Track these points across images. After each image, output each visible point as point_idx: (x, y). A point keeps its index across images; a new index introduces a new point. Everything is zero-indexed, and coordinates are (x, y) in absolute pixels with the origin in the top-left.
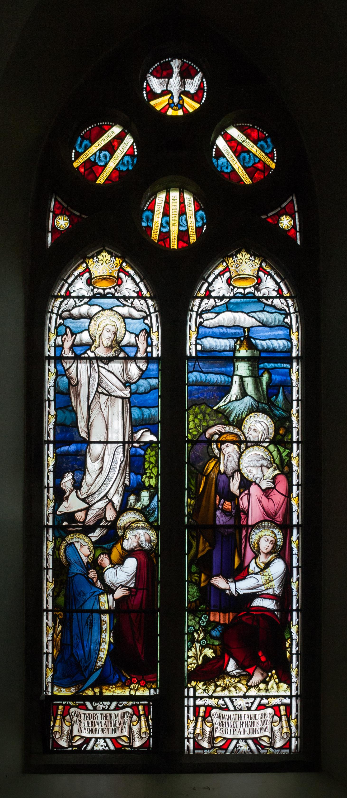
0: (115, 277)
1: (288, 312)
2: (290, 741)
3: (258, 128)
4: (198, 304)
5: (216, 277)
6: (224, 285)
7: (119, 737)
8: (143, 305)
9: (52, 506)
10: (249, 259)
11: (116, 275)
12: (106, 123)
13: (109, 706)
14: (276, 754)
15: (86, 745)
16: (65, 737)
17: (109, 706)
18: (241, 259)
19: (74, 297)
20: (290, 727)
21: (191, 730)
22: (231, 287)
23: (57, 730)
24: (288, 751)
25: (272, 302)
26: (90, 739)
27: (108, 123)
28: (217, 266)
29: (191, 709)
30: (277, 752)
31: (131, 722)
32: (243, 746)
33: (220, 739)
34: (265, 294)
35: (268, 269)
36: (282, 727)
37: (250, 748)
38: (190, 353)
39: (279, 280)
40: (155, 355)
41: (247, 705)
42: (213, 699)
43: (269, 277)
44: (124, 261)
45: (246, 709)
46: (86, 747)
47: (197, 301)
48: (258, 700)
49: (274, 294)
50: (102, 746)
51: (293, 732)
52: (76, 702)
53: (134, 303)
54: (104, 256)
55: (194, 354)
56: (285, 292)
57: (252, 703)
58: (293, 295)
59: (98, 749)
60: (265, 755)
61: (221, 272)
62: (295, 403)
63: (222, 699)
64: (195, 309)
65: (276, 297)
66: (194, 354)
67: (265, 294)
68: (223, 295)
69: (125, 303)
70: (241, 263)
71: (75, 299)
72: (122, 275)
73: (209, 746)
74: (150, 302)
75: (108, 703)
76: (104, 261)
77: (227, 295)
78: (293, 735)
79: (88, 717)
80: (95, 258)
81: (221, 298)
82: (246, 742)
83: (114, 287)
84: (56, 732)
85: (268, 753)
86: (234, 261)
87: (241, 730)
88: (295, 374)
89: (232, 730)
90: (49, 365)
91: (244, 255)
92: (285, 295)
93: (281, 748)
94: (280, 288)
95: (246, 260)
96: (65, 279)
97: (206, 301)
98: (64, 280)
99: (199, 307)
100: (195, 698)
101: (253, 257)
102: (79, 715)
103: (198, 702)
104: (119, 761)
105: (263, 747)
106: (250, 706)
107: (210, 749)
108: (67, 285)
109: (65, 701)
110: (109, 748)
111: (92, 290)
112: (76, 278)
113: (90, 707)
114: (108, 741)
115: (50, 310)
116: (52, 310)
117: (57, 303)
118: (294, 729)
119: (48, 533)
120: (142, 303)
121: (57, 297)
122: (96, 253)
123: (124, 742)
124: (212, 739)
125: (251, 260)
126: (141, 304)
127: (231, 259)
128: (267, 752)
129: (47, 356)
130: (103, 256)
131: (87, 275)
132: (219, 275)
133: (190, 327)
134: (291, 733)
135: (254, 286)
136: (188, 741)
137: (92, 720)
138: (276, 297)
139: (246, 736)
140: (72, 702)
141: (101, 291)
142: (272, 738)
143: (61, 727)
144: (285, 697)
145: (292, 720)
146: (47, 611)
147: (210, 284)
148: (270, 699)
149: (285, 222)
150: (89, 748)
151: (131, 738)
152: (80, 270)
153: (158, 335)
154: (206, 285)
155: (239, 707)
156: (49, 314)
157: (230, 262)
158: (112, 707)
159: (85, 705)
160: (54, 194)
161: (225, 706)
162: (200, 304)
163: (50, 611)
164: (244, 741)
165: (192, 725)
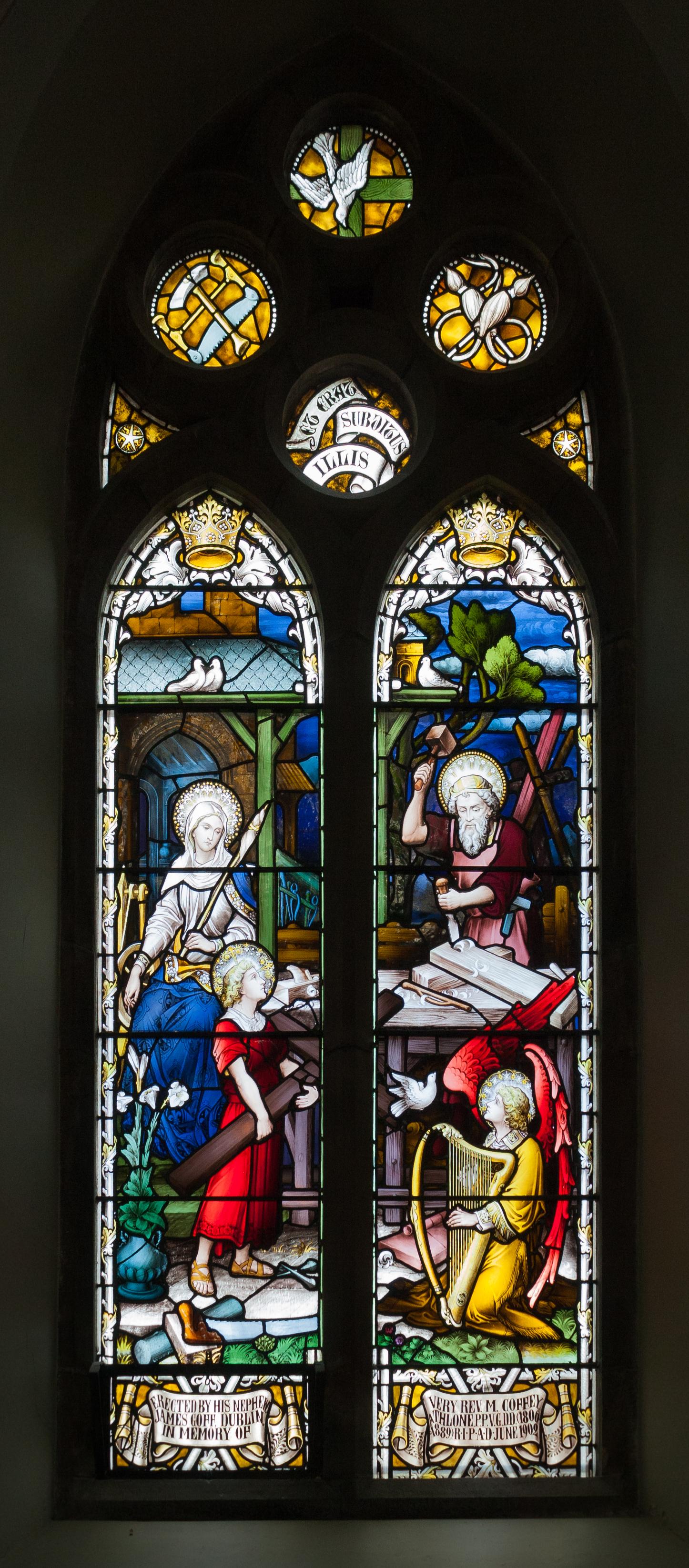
1: (296, 616)
2: (577, 1450)
4: (395, 601)
5: (431, 548)
6: (448, 564)
8: (560, 601)
9: (113, 994)
13: (223, 1386)
14: (551, 1478)
15: (181, 1461)
17: (223, 1386)
18: (204, 514)
19: (152, 589)
20: (577, 1426)
21: (385, 1432)
23: (401, 1435)
24: (572, 1473)
26: (190, 1449)
28: (156, 531)
29: (385, 1390)
30: (553, 1474)
31: (268, 1416)
33: (164, 1448)
37: (499, 1467)
38: (379, 698)
39: (277, 556)
40: (311, 700)
41: (494, 1382)
42: (427, 1370)
43: (259, 550)
44: (249, 518)
45: (491, 1390)
46: (182, 1465)
47: (121, 596)
48: (515, 1371)
49: (270, 582)
51: (583, 1434)
52: (160, 1378)
53: (268, 598)
54: (484, 505)
55: (386, 698)
56: (565, 578)
57: (504, 1378)
58: (304, 583)
59: (204, 1469)
60: (530, 1480)
61: (439, 538)
62: (585, 794)
63: (443, 1371)
64: (391, 611)
66: (386, 698)
68: (445, 582)
69: (525, 596)
70: (479, 521)
71: (155, 593)
73: (420, 1463)
74: (574, 596)
75: (222, 1379)
76: (484, 514)
77: (452, 581)
78: (584, 1441)
79: (189, 1406)
81: (441, 588)
82: (492, 1454)
85: (535, 1476)
89: (467, 1430)
90: (105, 719)
91: (210, 507)
92: (564, 585)
93: (560, 1466)
95: (215, 518)
96: (134, 551)
97: (411, 593)
98: (131, 553)
99: (399, 605)
100: (393, 1368)
101: (228, 510)
103: (399, 1377)
106: (498, 1383)
107: (422, 1468)
108: (137, 565)
109: (137, 1375)
110: (225, 1467)
111: (188, 575)
112: (154, 552)
113: (186, 1388)
114: (223, 1452)
115: (106, 612)
118: (584, 1430)
119: (104, 1047)
120: (284, 598)
121: (119, 588)
122: (194, 500)
123: (255, 1455)
125: (498, 516)
126: (557, 600)
127: (186, 514)
129: (101, 702)
130: (207, 507)
133: (105, 649)
134: (580, 1438)
135: (503, 566)
140: (150, 1378)
142: (267, 1447)
144: (567, 1366)
146: (104, 1199)
148: (537, 1372)
149: (566, 444)
150: (188, 1465)
151: (267, 1447)
152: (163, 535)
153: (317, 661)
154: (413, 562)
155: (478, 1387)
156: (105, 619)
157: (183, 521)
158: (230, 1388)
159: (175, 1382)
161: (451, 1385)
163: (109, 1199)
164: (488, 1451)
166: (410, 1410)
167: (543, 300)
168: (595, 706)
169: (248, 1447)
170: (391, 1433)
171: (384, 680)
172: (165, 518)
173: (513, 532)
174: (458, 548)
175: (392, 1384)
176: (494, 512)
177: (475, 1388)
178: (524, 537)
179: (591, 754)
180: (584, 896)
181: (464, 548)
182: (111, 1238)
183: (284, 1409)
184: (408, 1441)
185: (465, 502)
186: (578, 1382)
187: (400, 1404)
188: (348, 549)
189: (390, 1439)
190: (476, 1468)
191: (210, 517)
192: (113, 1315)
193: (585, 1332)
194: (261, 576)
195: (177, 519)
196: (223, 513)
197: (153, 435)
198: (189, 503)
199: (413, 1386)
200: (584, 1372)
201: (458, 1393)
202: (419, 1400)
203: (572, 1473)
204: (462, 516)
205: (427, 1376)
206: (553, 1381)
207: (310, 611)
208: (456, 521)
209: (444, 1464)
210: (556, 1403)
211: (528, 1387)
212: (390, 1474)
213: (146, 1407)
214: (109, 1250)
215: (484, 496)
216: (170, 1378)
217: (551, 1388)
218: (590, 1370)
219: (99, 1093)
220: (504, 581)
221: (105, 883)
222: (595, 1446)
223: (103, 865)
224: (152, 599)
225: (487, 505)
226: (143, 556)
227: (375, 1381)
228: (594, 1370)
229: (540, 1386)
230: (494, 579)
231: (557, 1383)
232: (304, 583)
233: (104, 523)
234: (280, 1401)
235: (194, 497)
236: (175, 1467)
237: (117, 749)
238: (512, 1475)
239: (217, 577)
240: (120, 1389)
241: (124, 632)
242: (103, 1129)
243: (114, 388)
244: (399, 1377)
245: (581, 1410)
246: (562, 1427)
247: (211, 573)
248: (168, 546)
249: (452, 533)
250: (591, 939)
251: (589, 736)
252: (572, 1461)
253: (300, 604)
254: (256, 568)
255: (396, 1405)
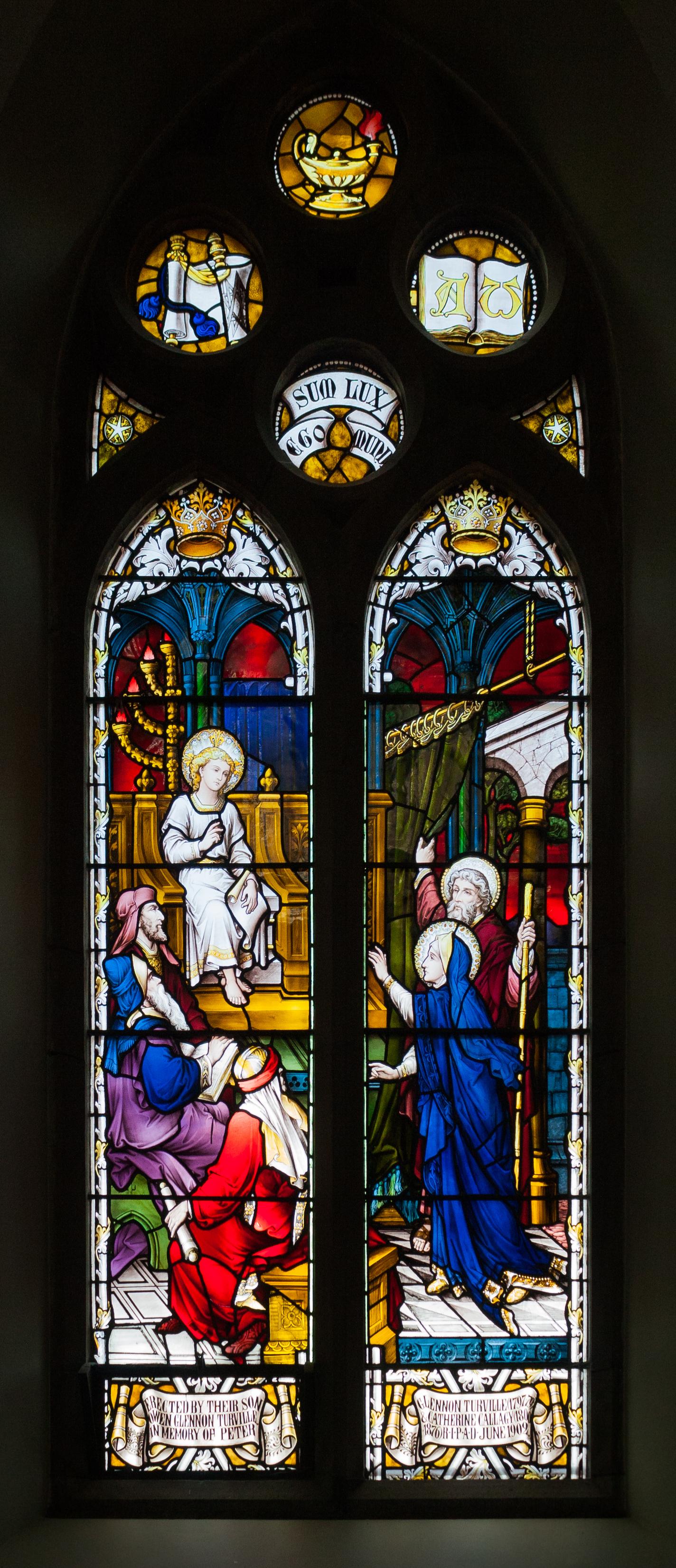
0: (222, 538)
1: (563, 605)
2: (568, 1451)
3: (497, 237)
6: (164, 555)
7: (511, 1445)
10: (212, 503)
11: (223, 531)
12: (482, 233)
13: (220, 1386)
15: (175, 1462)
16: (134, 1445)
17: (220, 1386)
20: (568, 1425)
21: (377, 1430)
22: (176, 557)
25: (257, 589)
27: (487, 234)
29: (378, 1389)
30: (544, 1474)
31: (262, 1415)
32: (479, 1463)
34: (517, 570)
35: (522, 520)
36: (553, 1425)
37: (491, 1466)
38: (371, 688)
39: (268, 544)
40: (300, 693)
41: (485, 1382)
43: (250, 539)
45: (483, 1390)
49: (261, 573)
50: (207, 1464)
52: (156, 1379)
54: (475, 492)
57: (495, 1378)
61: (429, 524)
64: (382, 602)
65: (538, 578)
66: (377, 689)
67: (517, 570)
70: (470, 507)
72: (235, 533)
74: (567, 587)
75: (218, 1380)
78: (574, 1441)
80: (183, 499)
81: (156, 581)
82: (484, 1453)
83: (494, 554)
84: (391, 1437)
86: (488, 503)
87: (469, 1430)
88: (577, 731)
91: (201, 495)
93: (550, 1465)
94: (547, 558)
95: (481, 504)
99: (389, 594)
101: (494, 496)
102: (161, 1405)
104: (235, 1493)
105: (517, 1464)
106: (490, 1383)
110: (220, 1467)
111: (179, 563)
112: (420, 535)
113: (182, 1388)
115: (372, 600)
116: (376, 599)
117: (109, 591)
118: (575, 1431)
119: (95, 714)
122: (184, 489)
124: (419, 1447)
126: (274, 591)
127: (176, 502)
128: (526, 1473)
131: (168, 533)
132: (428, 530)
134: (570, 1436)
136: (372, 1452)
137: (190, 1413)
138: (538, 578)
139: (484, 1442)
140: (148, 1379)
141: (196, 565)
143: (400, 1428)
145: (572, 1410)
146: (97, 866)
147: (134, 553)
149: (556, 429)
150: (183, 1467)
151: (261, 1447)
152: (430, 519)
153: (308, 655)
155: (470, 1387)
157: (175, 508)
159: (171, 1383)
160: (573, 377)
161: (442, 1384)
162: (391, 589)
163: (101, 866)
164: (480, 1451)
165: (379, 1421)
166: (403, 1409)
167: (535, 299)
168: (587, 698)
169: (244, 1447)
170: (383, 1432)
171: (376, 671)
172: (157, 505)
173: (505, 518)
174: (449, 535)
175: (384, 1384)
176: (485, 499)
177: (467, 1387)
178: (515, 523)
179: (583, 745)
180: (575, 891)
181: (455, 534)
182: (103, 820)
183: (278, 1407)
184: (401, 1440)
185: (456, 489)
186: (568, 1381)
187: (392, 1402)
188: (339, 532)
189: (382, 1438)
190: (468, 1467)
191: (476, 502)
192: (105, 813)
193: (575, 1246)
194: (528, 561)
195: (169, 507)
196: (215, 501)
197: (142, 425)
198: (178, 492)
199: (405, 1385)
200: (575, 1372)
201: (450, 1392)
202: (410, 1401)
203: (562, 1474)
204: (453, 503)
205: (417, 1376)
206: (543, 1381)
207: (302, 601)
208: (447, 509)
209: (437, 1464)
210: (547, 1404)
211: (519, 1386)
212: (383, 1474)
213: (140, 1406)
214: (102, 832)
215: (475, 482)
216: (168, 1379)
217: (542, 1387)
218: (581, 1370)
219: (92, 1087)
220: (220, 572)
221: (96, 879)
222: (586, 1446)
223: (95, 860)
224: (142, 588)
225: (478, 492)
226: (134, 546)
227: (368, 1381)
228: (585, 1370)
229: (533, 1385)
230: (210, 570)
231: (548, 1383)
232: (297, 575)
233: (92, 519)
234: (275, 1402)
235: (184, 486)
236: (169, 1469)
237: (107, 744)
238: (504, 1477)
239: (208, 565)
240: (114, 1388)
241: (114, 623)
242: (96, 795)
243: (100, 380)
244: (391, 1376)
245: (572, 1410)
246: (553, 1425)
247: (201, 562)
248: (434, 530)
249: (443, 519)
250: (582, 851)
251: (580, 894)
252: (563, 1461)
253: (292, 592)
254: (523, 556)
255: (388, 1404)
